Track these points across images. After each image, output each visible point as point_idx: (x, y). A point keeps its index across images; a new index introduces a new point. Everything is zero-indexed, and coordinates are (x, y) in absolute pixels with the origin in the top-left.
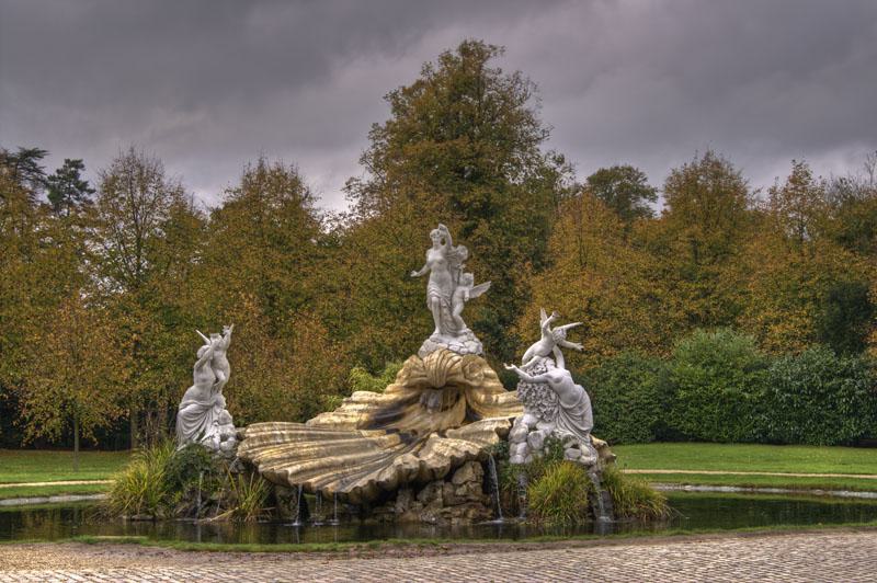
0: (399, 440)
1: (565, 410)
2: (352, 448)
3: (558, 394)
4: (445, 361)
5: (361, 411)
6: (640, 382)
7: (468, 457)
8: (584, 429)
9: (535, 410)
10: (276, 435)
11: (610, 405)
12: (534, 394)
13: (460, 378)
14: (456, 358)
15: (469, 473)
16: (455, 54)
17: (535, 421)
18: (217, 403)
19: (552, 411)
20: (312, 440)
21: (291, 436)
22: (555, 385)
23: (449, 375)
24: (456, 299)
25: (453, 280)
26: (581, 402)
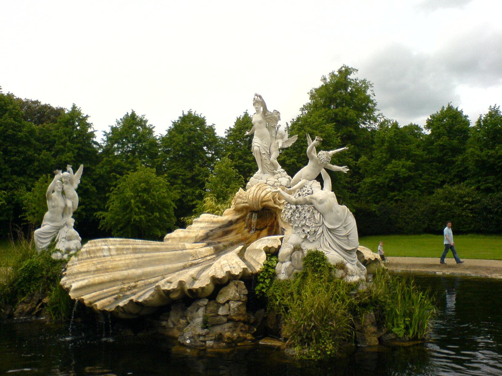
0: (212, 252)
1: (330, 230)
2: (165, 259)
3: (322, 215)
4: (260, 192)
5: (202, 228)
6: (418, 209)
7: (231, 278)
8: (349, 248)
9: (300, 231)
10: (103, 249)
11: (405, 219)
12: (298, 215)
13: (271, 204)
14: (269, 190)
15: (231, 292)
16: (336, 73)
17: (300, 241)
18: (66, 224)
19: (315, 232)
20: (136, 253)
21: (117, 249)
22: (319, 207)
23: (262, 202)
24: (272, 149)
25: (271, 136)
26: (345, 222)
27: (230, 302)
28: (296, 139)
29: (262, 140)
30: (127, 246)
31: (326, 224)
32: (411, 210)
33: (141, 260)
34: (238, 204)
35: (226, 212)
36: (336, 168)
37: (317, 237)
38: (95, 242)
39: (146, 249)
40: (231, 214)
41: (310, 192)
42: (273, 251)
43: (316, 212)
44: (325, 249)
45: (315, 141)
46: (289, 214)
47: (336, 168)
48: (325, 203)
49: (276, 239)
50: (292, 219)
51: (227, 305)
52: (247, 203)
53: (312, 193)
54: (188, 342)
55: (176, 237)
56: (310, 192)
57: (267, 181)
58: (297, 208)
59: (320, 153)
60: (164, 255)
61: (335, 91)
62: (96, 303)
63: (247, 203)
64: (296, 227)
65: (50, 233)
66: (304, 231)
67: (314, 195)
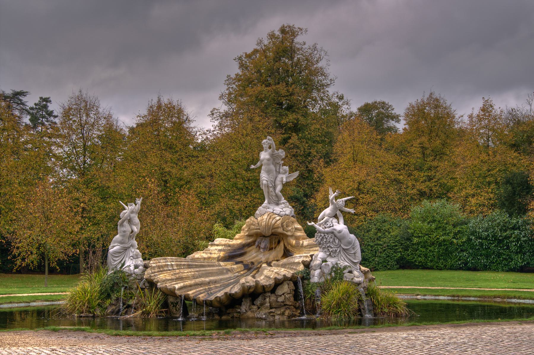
1: (344, 249)
3: (340, 240)
5: (220, 250)
7: (285, 279)
9: (326, 250)
10: (168, 265)
13: (280, 230)
16: (277, 33)
17: (326, 256)
18: (132, 246)
21: (177, 265)
22: (338, 235)
23: (273, 229)
25: (276, 171)
27: (285, 294)
28: (298, 175)
29: (268, 175)
30: (183, 263)
31: (342, 245)
32: (379, 234)
33: (200, 272)
34: (252, 230)
35: (237, 236)
36: (347, 210)
37: (337, 254)
38: (157, 260)
39: (196, 265)
40: (242, 238)
41: (332, 225)
42: (306, 263)
43: (336, 238)
44: (342, 261)
45: (336, 193)
46: (320, 239)
47: (347, 210)
48: (341, 234)
49: (307, 256)
50: (322, 242)
51: (283, 296)
52: (259, 229)
53: (333, 226)
54: (264, 316)
55: (200, 257)
56: (332, 225)
57: (274, 210)
58: (324, 235)
59: (338, 200)
60: (212, 270)
61: (277, 59)
62: (199, 296)
63: (259, 229)
64: (323, 248)
65: (120, 252)
66: (328, 250)
67: (335, 227)
